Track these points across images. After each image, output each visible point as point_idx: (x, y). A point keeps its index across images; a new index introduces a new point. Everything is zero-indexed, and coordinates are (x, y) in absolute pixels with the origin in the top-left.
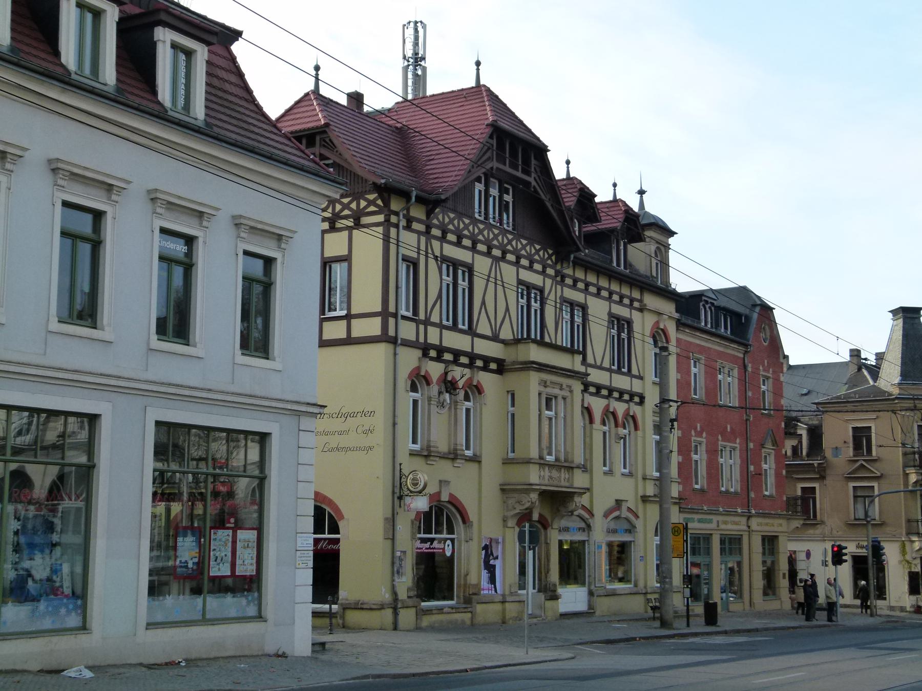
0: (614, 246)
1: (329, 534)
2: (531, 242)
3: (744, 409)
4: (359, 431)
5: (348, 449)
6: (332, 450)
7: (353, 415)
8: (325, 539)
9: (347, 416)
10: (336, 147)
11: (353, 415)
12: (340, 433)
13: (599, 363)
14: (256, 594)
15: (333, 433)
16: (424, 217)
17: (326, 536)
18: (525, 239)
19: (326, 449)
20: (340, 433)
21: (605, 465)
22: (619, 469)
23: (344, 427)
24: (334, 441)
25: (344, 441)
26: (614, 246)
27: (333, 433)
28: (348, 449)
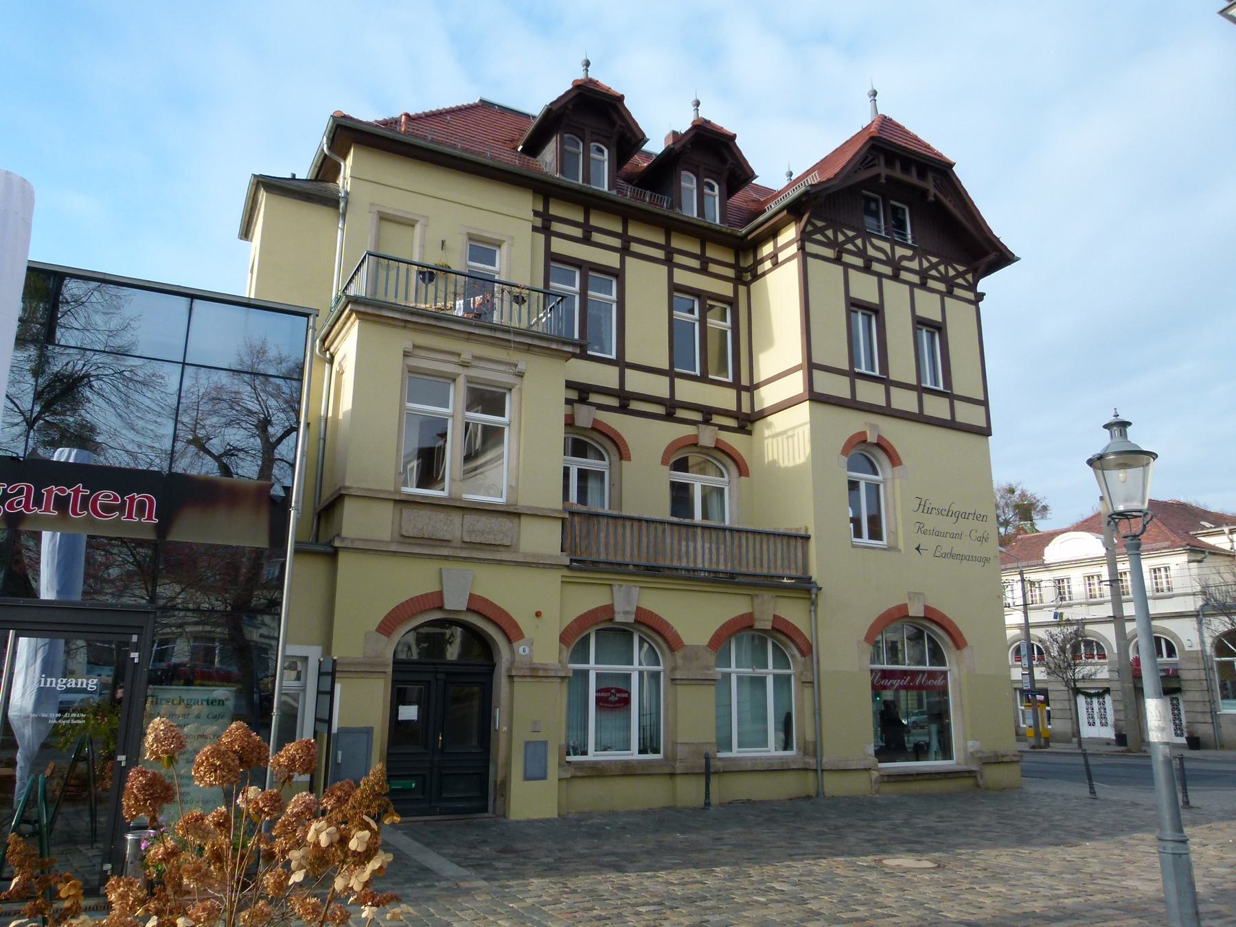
0: (750, 237)
1: (930, 665)
2: (947, 261)
3: (811, 775)
4: (974, 535)
5: (962, 558)
6: (945, 556)
7: (965, 516)
8: (923, 672)
9: (959, 515)
10: (865, 169)
11: (965, 516)
12: (953, 536)
13: (644, 524)
14: (916, 711)
15: (944, 535)
16: (619, 229)
17: (927, 667)
18: (934, 255)
19: (938, 554)
20: (953, 536)
21: (1049, 712)
22: (1097, 721)
23: (954, 529)
24: (947, 544)
25: (961, 547)
26: (750, 237)
27: (944, 535)
28: (962, 558)
